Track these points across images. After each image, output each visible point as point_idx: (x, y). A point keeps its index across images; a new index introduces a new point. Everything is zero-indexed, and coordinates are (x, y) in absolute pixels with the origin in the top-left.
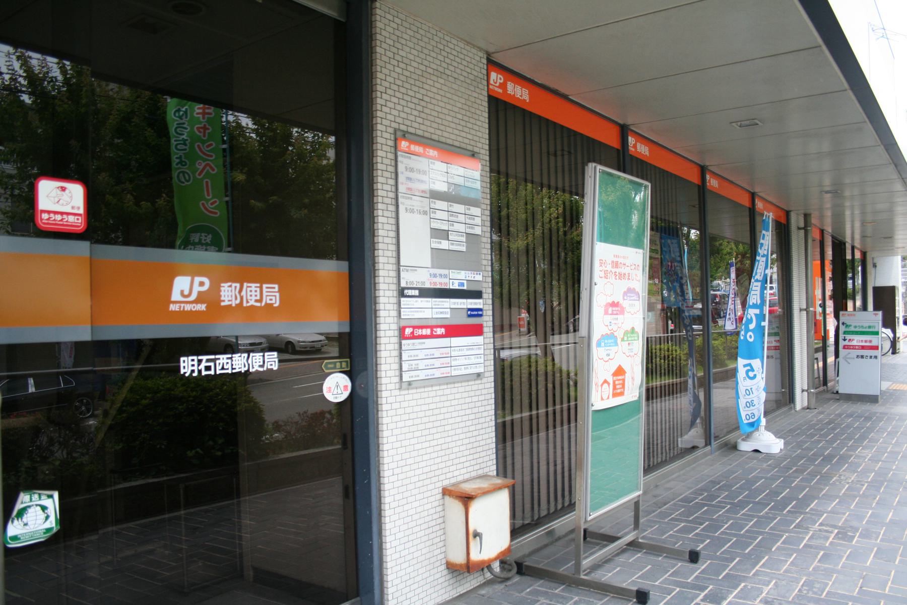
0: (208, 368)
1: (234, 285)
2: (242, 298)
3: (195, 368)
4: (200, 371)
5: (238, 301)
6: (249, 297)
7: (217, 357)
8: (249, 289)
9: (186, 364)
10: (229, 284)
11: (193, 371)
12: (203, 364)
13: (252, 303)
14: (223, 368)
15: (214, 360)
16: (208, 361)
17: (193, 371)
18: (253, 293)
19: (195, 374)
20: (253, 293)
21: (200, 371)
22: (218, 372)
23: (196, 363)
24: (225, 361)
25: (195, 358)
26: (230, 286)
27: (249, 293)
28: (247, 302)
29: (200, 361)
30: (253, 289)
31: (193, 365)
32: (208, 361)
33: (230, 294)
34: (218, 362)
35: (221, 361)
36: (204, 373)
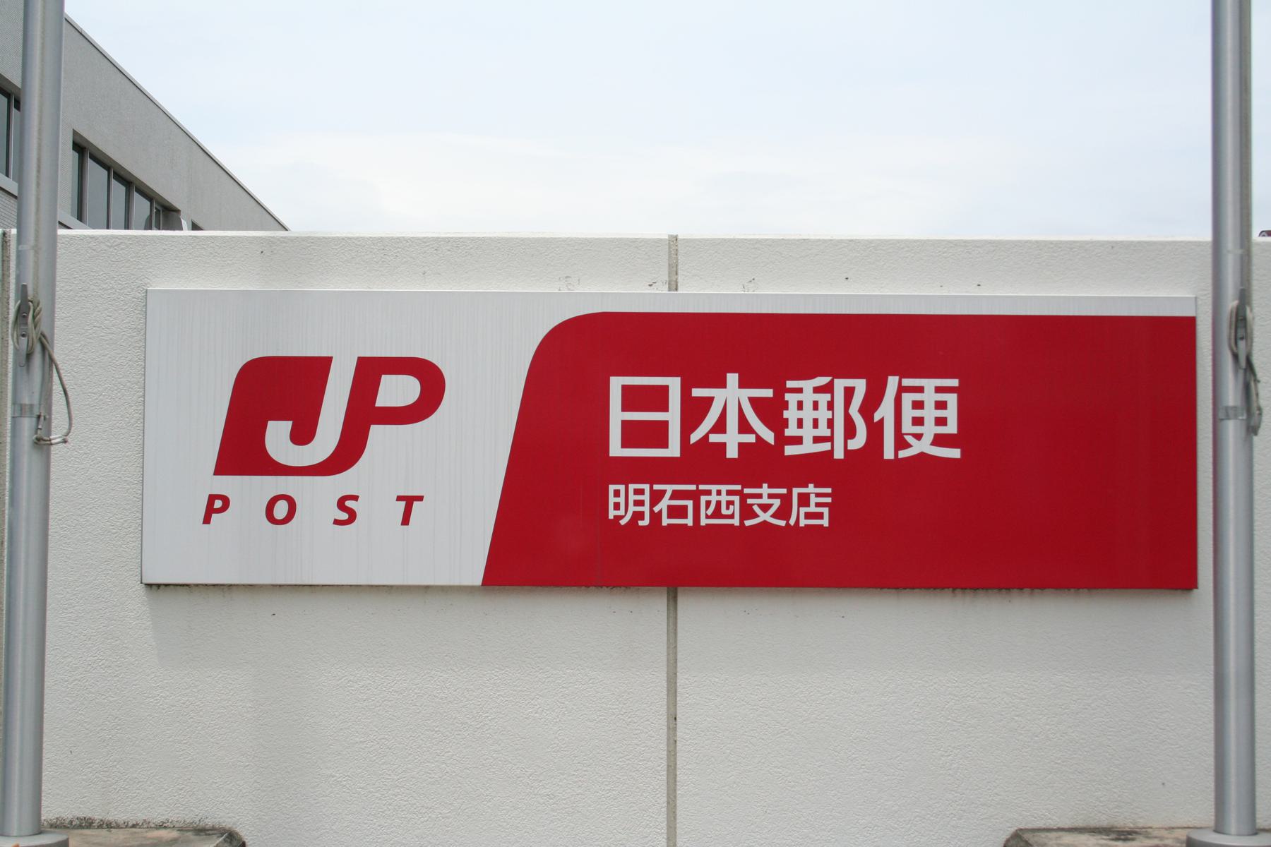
0: (676, 512)
1: (840, 384)
2: (875, 430)
3: (646, 509)
4: (656, 517)
5: (858, 442)
6: (907, 427)
7: (702, 487)
8: (908, 399)
9: (621, 500)
10: (822, 381)
11: (639, 515)
12: (663, 505)
13: (923, 446)
14: (717, 514)
15: (695, 496)
16: (676, 495)
17: (639, 515)
18: (808, 414)
19: (645, 522)
20: (808, 414)
21: (656, 517)
22: (704, 521)
23: (646, 497)
24: (724, 498)
25: (646, 487)
26: (828, 389)
27: (908, 413)
28: (901, 443)
29: (656, 497)
30: (929, 397)
31: (639, 503)
32: (676, 495)
33: (823, 415)
34: (703, 499)
35: (714, 498)
36: (666, 521)
